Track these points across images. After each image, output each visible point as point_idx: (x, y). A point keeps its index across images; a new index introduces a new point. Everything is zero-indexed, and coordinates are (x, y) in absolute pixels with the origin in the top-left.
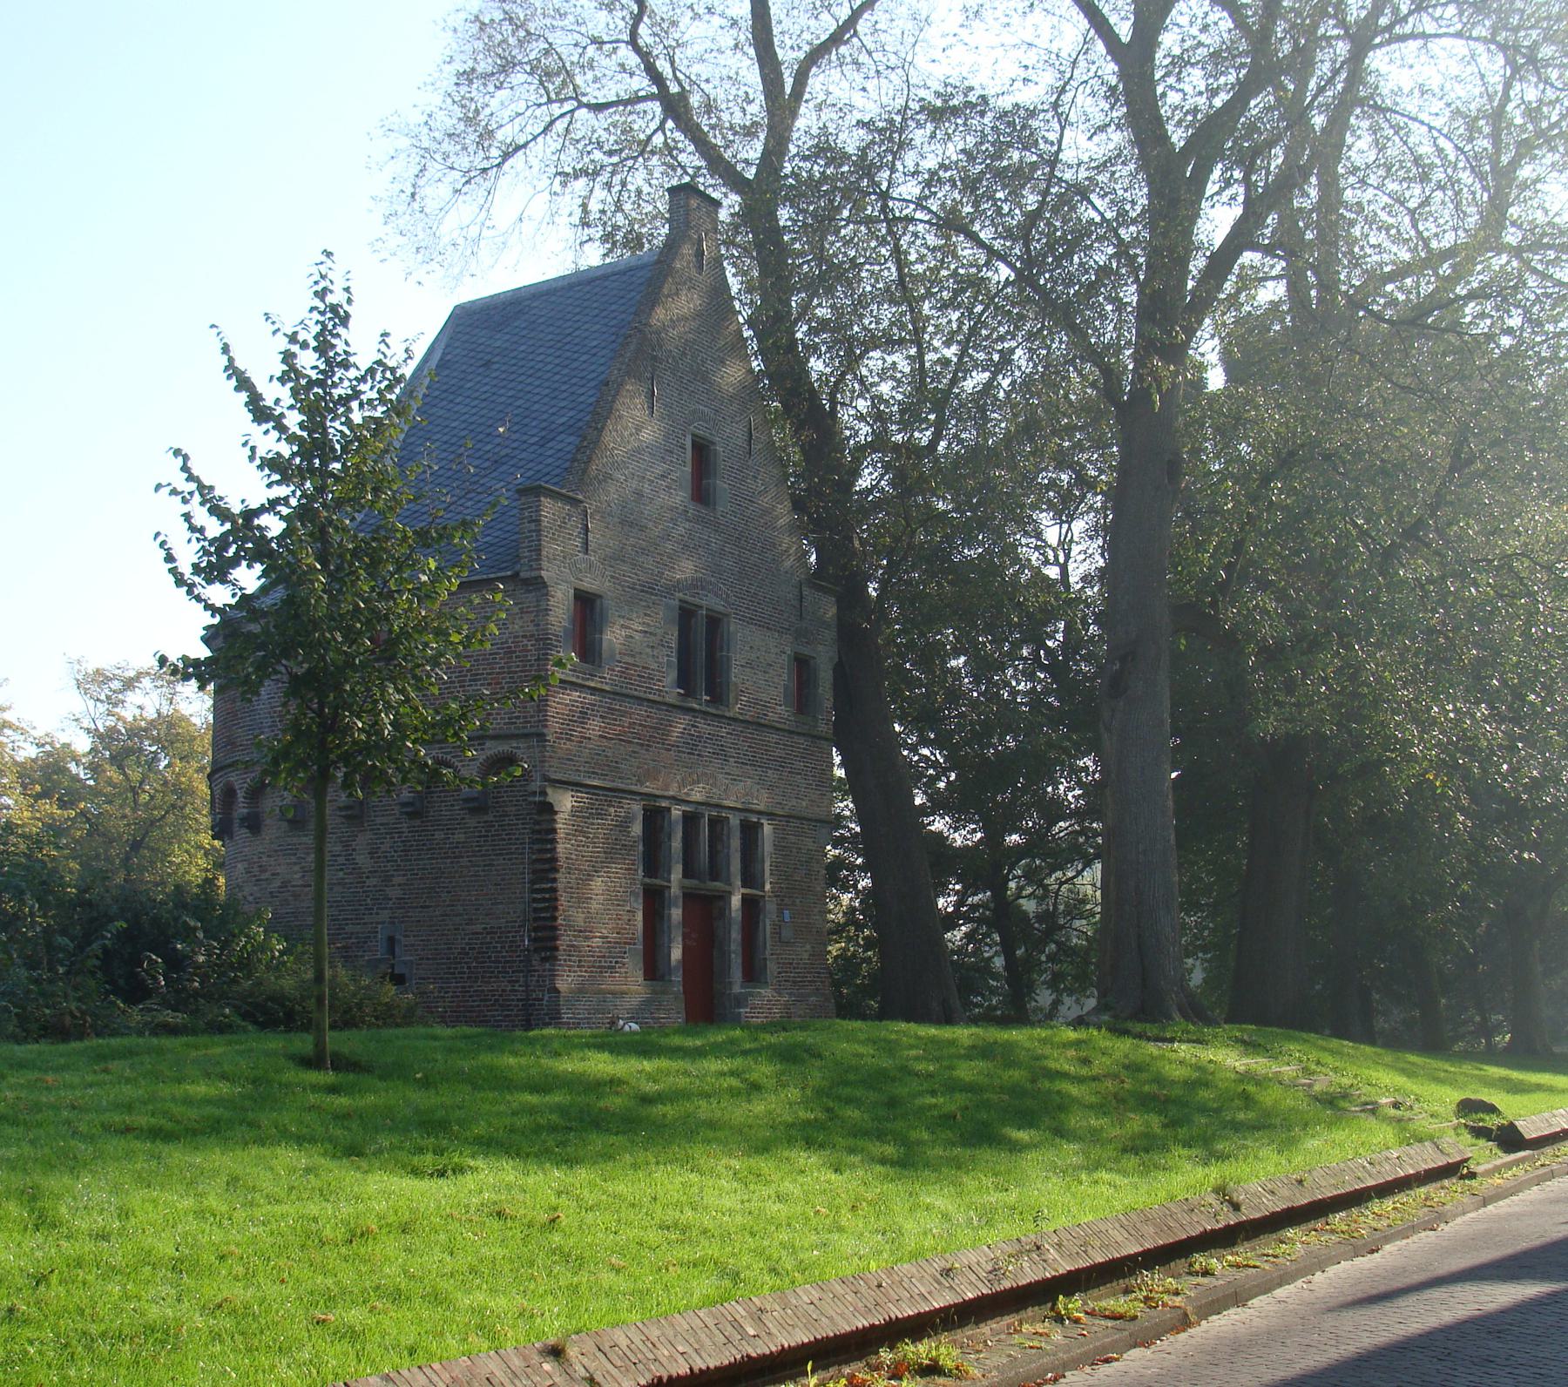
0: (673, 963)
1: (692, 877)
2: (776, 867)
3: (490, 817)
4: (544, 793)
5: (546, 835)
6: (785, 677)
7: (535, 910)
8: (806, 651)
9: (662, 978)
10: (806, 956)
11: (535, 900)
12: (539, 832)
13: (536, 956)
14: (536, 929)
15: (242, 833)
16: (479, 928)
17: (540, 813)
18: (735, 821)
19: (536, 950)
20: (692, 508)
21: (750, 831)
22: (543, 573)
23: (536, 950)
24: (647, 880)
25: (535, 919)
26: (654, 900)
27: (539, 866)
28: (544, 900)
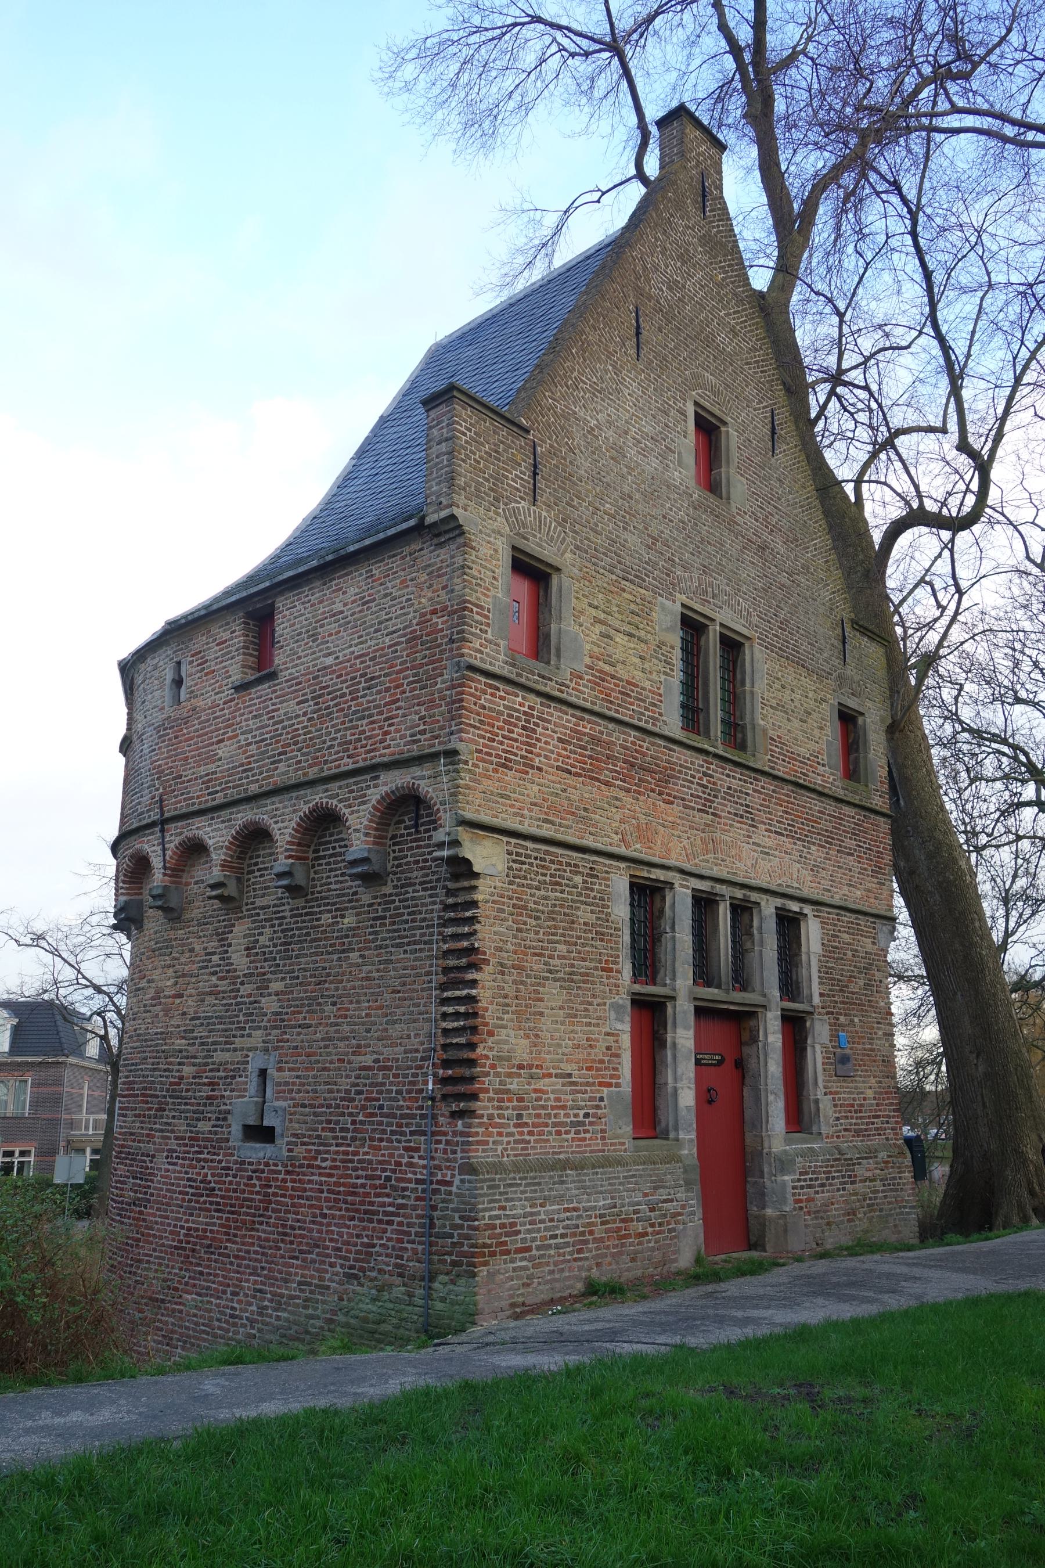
0: (683, 1112)
1: (708, 984)
2: (826, 972)
3: (388, 890)
4: (456, 843)
5: (461, 911)
6: (828, 731)
7: (446, 1032)
8: (852, 703)
9: (664, 1135)
10: (870, 1093)
11: (445, 1016)
12: (454, 907)
13: (444, 1109)
14: (446, 1064)
15: (154, 921)
16: (368, 1060)
17: (456, 877)
18: (769, 907)
19: (444, 1097)
20: (698, 494)
21: (789, 925)
22: (458, 512)
23: (444, 1097)
24: (638, 988)
25: (445, 1047)
26: (650, 1014)
27: (452, 962)
28: (457, 1015)
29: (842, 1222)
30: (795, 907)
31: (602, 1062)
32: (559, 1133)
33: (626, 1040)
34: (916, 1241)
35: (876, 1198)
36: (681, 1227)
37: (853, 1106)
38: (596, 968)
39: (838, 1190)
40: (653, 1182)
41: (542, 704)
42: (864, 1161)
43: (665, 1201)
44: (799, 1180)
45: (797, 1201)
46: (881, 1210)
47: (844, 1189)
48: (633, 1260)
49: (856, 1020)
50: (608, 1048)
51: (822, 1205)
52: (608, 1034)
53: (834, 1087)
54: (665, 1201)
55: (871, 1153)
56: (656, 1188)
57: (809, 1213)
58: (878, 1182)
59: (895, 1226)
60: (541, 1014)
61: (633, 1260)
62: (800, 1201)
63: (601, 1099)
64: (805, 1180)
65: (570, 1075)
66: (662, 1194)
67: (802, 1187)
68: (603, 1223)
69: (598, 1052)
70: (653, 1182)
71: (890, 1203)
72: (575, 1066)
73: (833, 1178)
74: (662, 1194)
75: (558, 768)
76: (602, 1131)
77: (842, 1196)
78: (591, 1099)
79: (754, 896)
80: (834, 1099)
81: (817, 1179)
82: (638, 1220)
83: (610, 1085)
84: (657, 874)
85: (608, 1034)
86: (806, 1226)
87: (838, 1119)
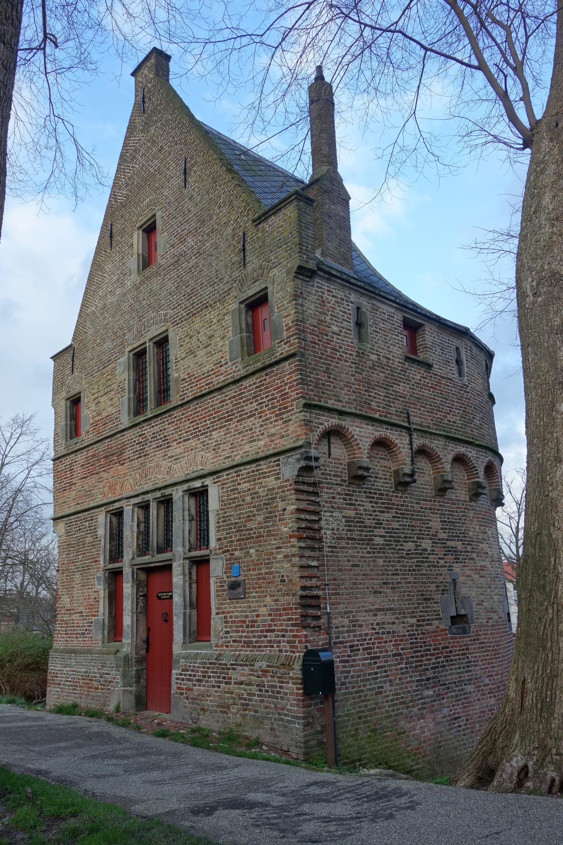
10: (263, 611)
24: (110, 566)
26: (115, 576)
29: (216, 712)
30: (197, 484)
31: (93, 605)
32: (77, 638)
33: (101, 593)
34: (296, 752)
35: (250, 700)
36: (112, 688)
37: (244, 622)
38: (92, 562)
39: (213, 686)
40: (102, 663)
41: (140, 428)
42: (239, 667)
43: (106, 674)
44: (181, 674)
45: (179, 688)
46: (256, 711)
47: (219, 687)
48: (93, 699)
49: (252, 551)
50: (95, 598)
51: (199, 695)
52: (95, 592)
53: (228, 607)
54: (106, 674)
55: (250, 662)
56: (103, 667)
57: (187, 698)
58: (255, 687)
59: (272, 729)
60: (73, 587)
61: (93, 699)
62: (182, 689)
63: (92, 622)
64: (185, 675)
65: (82, 612)
66: (105, 670)
67: (183, 680)
68: (83, 679)
69: (91, 601)
70: (102, 663)
71: (266, 707)
72: (84, 608)
73: (209, 677)
74: (105, 670)
75: (81, 479)
76: (91, 637)
77: (216, 692)
78: (88, 622)
79: (168, 491)
80: (226, 617)
81: (195, 676)
82: (96, 681)
83: (95, 616)
84: (117, 505)
85: (95, 592)
86: (185, 707)
87: (227, 632)
